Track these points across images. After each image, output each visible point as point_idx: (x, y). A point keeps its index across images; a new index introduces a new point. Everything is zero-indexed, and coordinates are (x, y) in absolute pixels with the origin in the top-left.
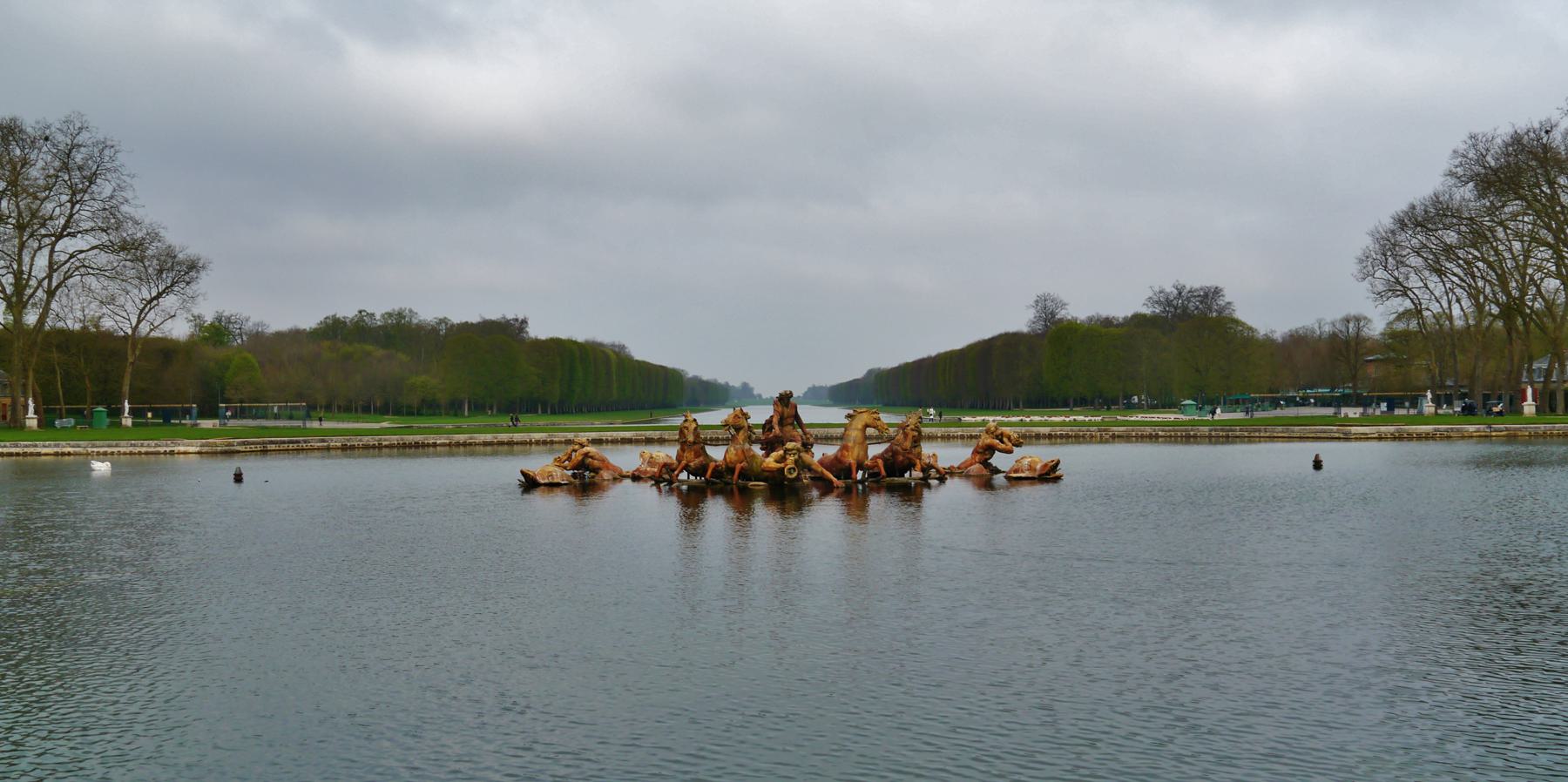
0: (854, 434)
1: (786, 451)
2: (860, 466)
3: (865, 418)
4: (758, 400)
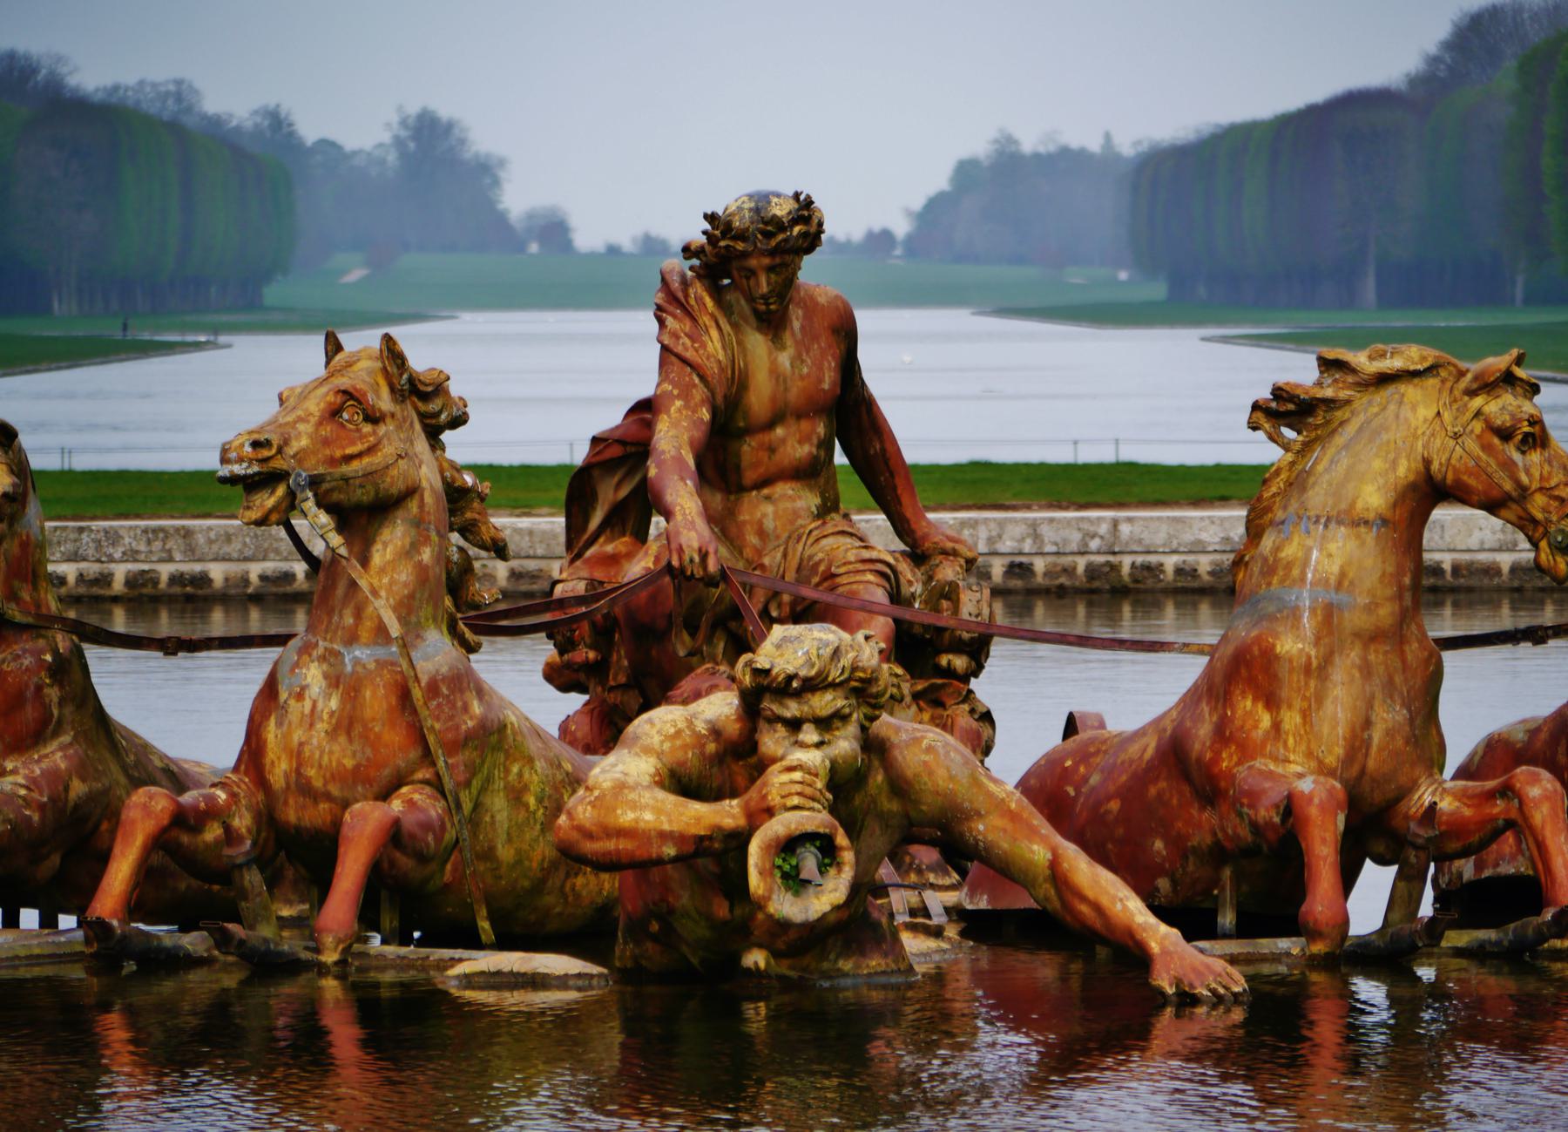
0: (1330, 558)
1: (762, 694)
2: (1373, 828)
4: (545, 270)
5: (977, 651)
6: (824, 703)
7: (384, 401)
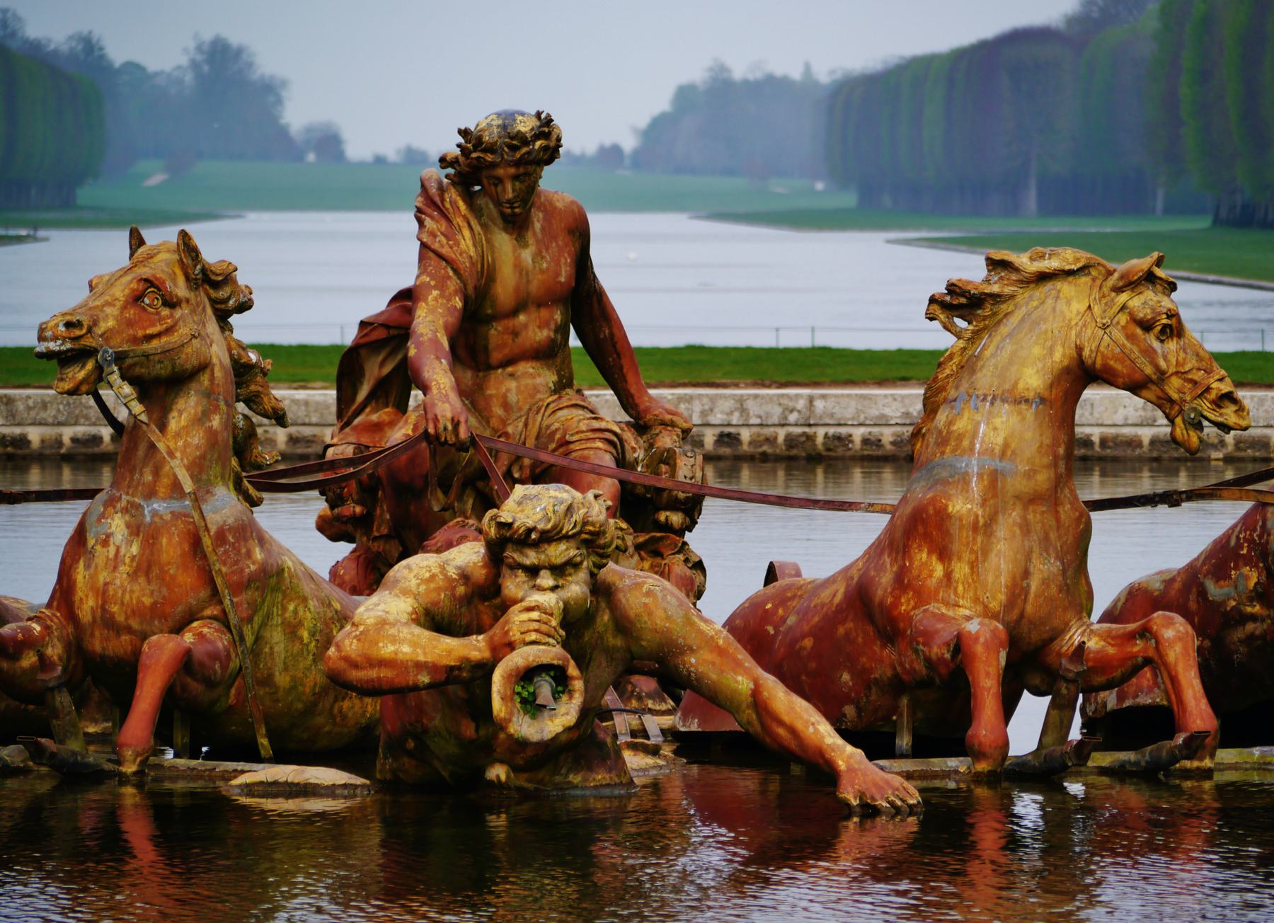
0: (996, 431)
1: (503, 546)
2: (1030, 664)
3: (1063, 320)
4: (319, 175)
5: (691, 508)
6: (559, 552)
7: (180, 289)
